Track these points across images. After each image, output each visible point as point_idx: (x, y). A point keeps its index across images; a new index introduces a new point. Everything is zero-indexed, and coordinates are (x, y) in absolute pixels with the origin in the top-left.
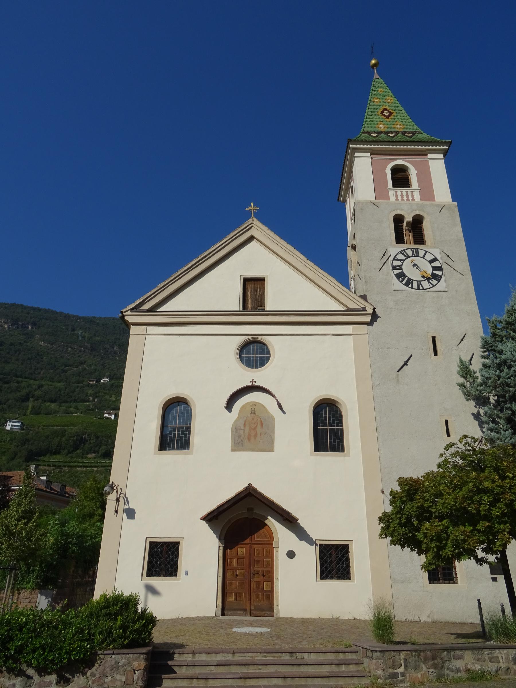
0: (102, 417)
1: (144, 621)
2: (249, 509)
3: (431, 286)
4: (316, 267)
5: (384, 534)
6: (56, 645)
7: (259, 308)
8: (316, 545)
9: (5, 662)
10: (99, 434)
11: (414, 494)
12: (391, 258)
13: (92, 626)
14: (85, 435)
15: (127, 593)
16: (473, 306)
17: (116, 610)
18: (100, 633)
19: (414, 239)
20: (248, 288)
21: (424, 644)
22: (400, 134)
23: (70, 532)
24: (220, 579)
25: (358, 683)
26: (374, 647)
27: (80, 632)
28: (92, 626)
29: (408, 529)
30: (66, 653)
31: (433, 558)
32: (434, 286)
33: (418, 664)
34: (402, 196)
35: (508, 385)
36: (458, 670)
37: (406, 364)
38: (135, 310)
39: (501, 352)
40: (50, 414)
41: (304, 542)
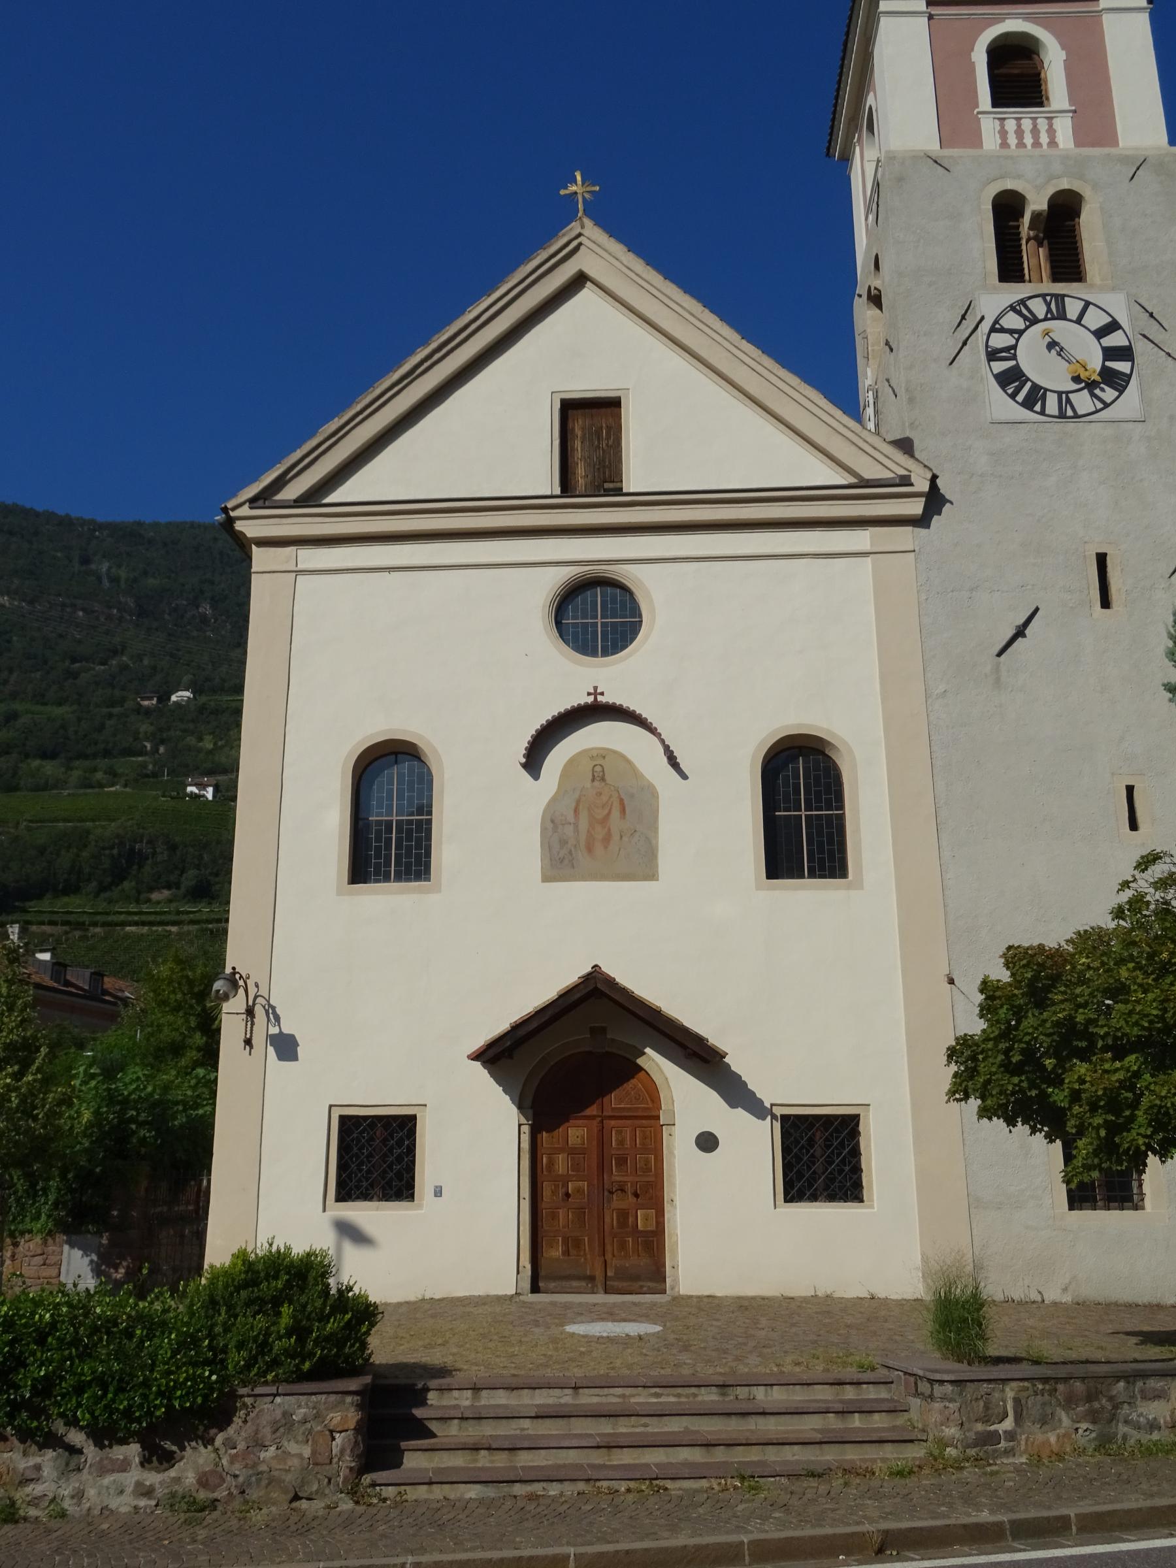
0: (181, 795)
1: (348, 1316)
2: (593, 1030)
3: (1100, 405)
4: (767, 361)
5: (960, 1090)
6: (132, 1376)
7: (607, 485)
8: (774, 1117)
9: (11, 1416)
10: (177, 839)
11: (1048, 989)
12: (985, 326)
13: (218, 1329)
14: (141, 841)
15: (299, 1249)
17: (276, 1289)
18: (240, 1346)
19: (1052, 268)
20: (573, 429)
21: (1064, 1363)
23: (130, 1094)
25: (895, 1456)
26: (936, 1371)
27: (191, 1343)
28: (218, 1329)
29: (1027, 1078)
30: (160, 1394)
31: (1096, 1153)
32: (1106, 405)
33: (1049, 1411)
34: (1019, 133)
36: (1153, 1426)
37: (1020, 633)
38: (260, 503)
41: (740, 1111)
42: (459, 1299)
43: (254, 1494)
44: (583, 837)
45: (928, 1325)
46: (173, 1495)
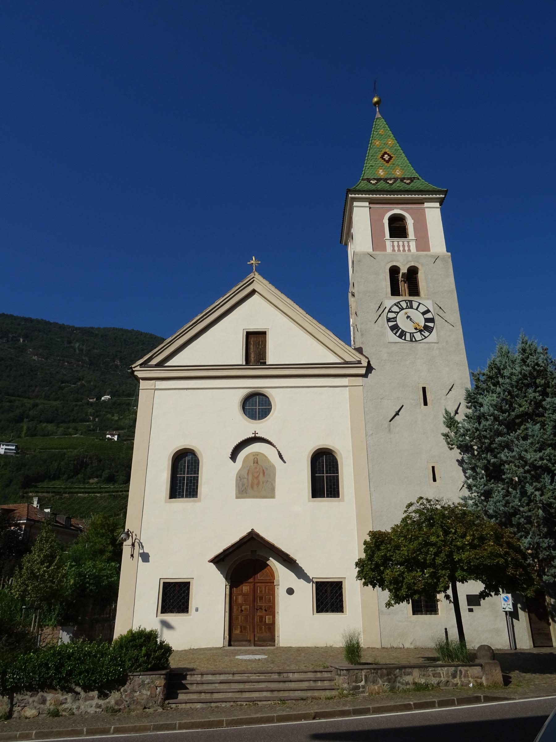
2: (252, 551)
3: (423, 337)
6: (97, 669)
7: (261, 361)
8: (313, 582)
11: (380, 545)
12: (387, 310)
13: (123, 655)
15: (148, 630)
16: (462, 357)
18: (129, 660)
22: (399, 180)
24: (227, 614)
28: (123, 655)
30: (105, 675)
32: (426, 337)
34: (398, 246)
35: (485, 437)
36: (407, 683)
37: (397, 414)
38: (143, 366)
39: (481, 405)
40: (47, 436)
42: (203, 649)
43: (132, 707)
44: (250, 482)
45: (345, 653)
46: (107, 707)
